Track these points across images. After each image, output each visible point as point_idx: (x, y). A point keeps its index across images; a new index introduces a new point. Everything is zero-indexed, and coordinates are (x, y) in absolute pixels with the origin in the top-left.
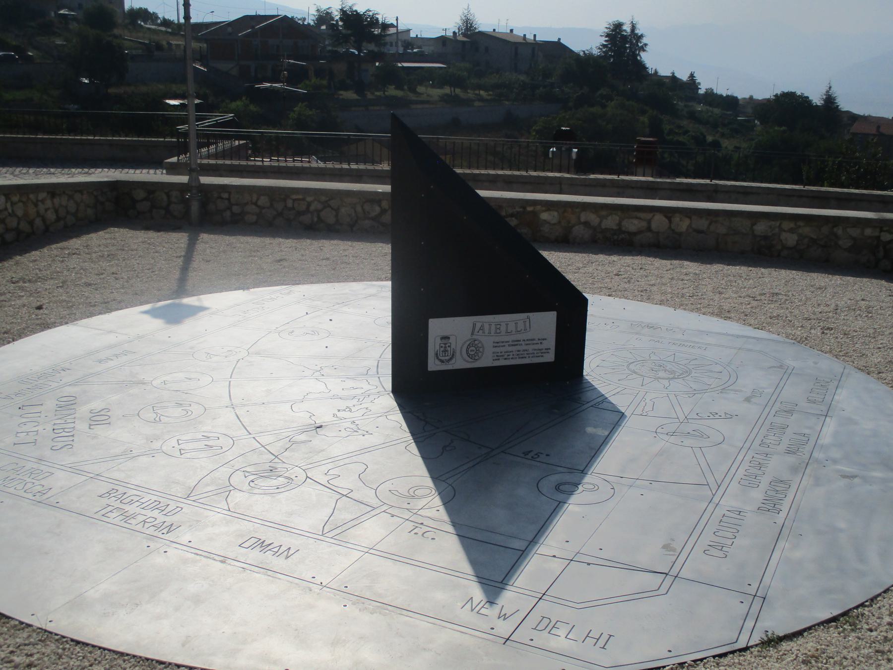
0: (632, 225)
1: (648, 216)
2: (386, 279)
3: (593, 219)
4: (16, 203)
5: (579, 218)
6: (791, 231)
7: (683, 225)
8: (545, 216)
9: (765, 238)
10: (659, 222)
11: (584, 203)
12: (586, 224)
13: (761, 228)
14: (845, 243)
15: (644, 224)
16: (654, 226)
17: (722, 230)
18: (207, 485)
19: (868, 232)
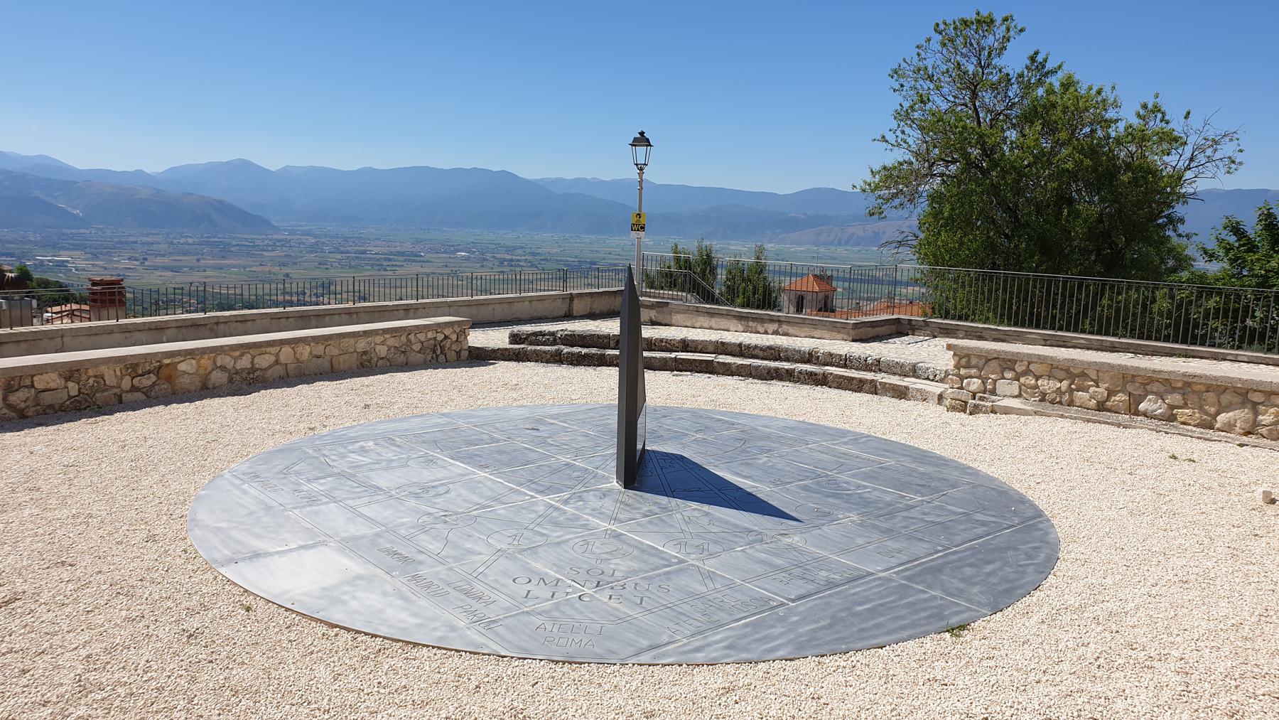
0: (264, 361)
1: (274, 350)
2: (667, 412)
3: (227, 361)
4: (995, 388)
5: (215, 363)
6: (383, 343)
7: (305, 352)
8: (182, 367)
9: (365, 353)
10: (286, 353)
11: (417, 326)
12: (223, 368)
13: (362, 345)
14: (417, 347)
15: (273, 358)
16: (282, 359)
17: (335, 352)
18: (983, 524)
19: (430, 335)
